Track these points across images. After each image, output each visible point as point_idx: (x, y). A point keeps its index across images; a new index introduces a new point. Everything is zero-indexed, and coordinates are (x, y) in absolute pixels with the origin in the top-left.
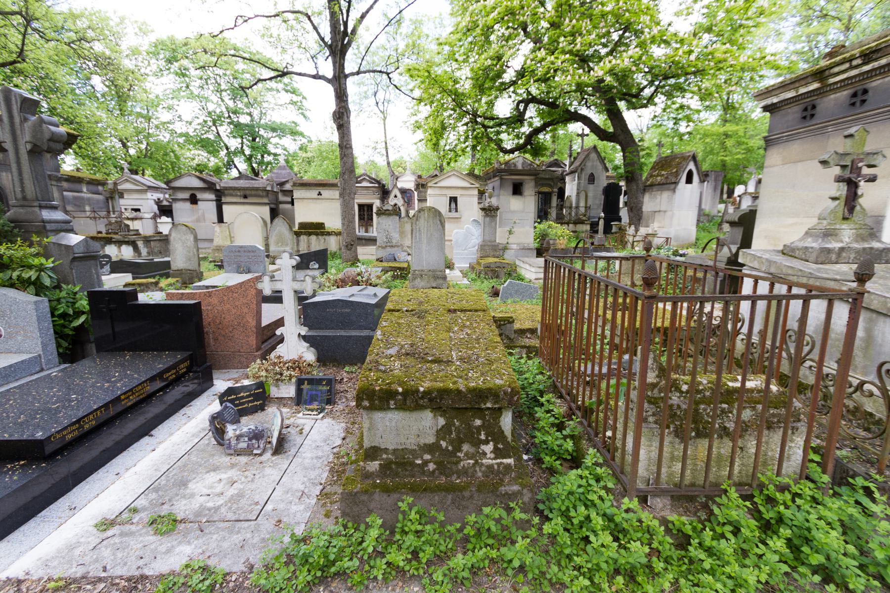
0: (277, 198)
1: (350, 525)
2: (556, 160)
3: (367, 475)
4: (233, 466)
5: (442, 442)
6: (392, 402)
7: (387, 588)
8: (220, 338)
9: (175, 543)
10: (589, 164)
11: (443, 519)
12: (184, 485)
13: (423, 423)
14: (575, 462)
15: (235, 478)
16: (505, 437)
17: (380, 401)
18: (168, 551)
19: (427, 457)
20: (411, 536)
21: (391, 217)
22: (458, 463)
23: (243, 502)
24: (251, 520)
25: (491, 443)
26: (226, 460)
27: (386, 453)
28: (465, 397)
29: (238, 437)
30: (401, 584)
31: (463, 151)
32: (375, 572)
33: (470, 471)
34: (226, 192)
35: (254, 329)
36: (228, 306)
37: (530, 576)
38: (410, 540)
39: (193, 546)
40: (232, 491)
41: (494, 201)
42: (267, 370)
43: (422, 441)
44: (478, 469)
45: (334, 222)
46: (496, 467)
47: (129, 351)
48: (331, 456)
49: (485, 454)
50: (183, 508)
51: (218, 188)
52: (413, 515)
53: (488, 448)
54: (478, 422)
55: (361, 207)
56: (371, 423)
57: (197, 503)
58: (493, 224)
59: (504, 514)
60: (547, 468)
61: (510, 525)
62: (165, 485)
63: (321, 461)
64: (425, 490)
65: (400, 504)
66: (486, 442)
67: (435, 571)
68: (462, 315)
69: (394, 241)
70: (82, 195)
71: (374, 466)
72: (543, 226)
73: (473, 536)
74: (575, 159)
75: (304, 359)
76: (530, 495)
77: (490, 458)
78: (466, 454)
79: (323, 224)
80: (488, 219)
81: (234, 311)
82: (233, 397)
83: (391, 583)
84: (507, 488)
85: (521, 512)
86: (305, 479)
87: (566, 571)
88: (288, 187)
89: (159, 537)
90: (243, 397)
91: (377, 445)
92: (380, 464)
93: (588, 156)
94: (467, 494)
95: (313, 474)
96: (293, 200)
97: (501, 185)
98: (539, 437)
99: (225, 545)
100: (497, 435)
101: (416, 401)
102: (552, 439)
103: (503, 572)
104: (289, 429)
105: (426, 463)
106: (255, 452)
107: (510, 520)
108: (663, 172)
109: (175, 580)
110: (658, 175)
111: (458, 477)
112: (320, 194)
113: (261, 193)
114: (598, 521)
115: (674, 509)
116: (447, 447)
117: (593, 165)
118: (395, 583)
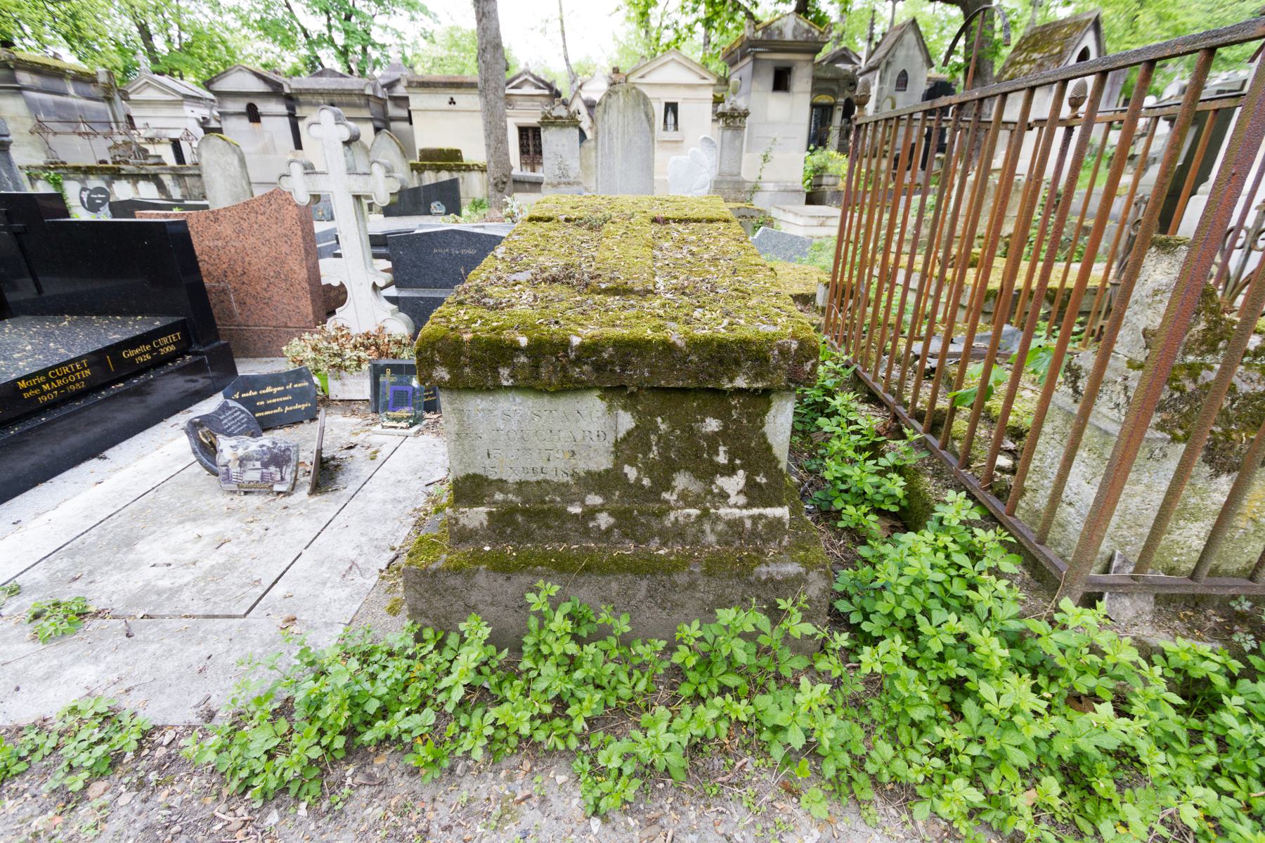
0: (385, 112)
1: (428, 633)
2: (845, 49)
3: (462, 536)
4: (231, 512)
5: (627, 469)
6: (504, 372)
7: (497, 772)
8: (248, 301)
9: (68, 658)
10: (901, 53)
11: (627, 629)
12: (128, 545)
13: (583, 424)
14: (907, 517)
15: (229, 535)
16: (774, 460)
17: (476, 370)
18: (48, 677)
19: (594, 500)
20: (548, 669)
21: (566, 131)
22: (662, 514)
23: (232, 579)
24: (234, 617)
25: (741, 472)
26: (223, 500)
27: (501, 491)
28: (684, 360)
29: (242, 461)
30: (527, 765)
31: (690, 29)
32: (467, 742)
33: (691, 531)
34: (301, 98)
35: (306, 285)
36: (252, 240)
37: (829, 769)
38: (550, 678)
39: (102, 667)
40: (218, 558)
41: (741, 103)
42: (315, 349)
43: (582, 466)
44: (707, 527)
45: (475, 152)
46: (748, 524)
47: (71, 314)
48: (423, 499)
49: (724, 496)
50: (111, 588)
51: (287, 90)
52: (559, 623)
53: (733, 484)
54: (712, 425)
55: (523, 131)
56: (461, 422)
57: (134, 582)
58: (737, 143)
59: (764, 622)
60: (846, 529)
61: (777, 646)
62: (94, 544)
63: (401, 507)
64: (587, 569)
65: (531, 597)
66: (730, 470)
67: (603, 746)
68: (680, 227)
69: (572, 174)
70: (69, 100)
71: (476, 516)
72: (818, 158)
73: (694, 668)
74: (878, 45)
75: (387, 331)
76: (822, 584)
77: (736, 506)
78: (683, 496)
79: (458, 151)
80: (729, 133)
81: (265, 249)
82: (251, 393)
83: (505, 763)
84: (773, 569)
85: (803, 620)
86: (363, 539)
87: (911, 754)
88: (400, 91)
89: (40, 646)
90: (271, 395)
91: (480, 471)
92: (490, 514)
93: (900, 38)
94: (681, 579)
95: (380, 531)
96: (409, 112)
97: (755, 72)
98: (832, 470)
99: (169, 666)
100: (753, 455)
101: (564, 369)
102: (862, 475)
103: (763, 750)
104: (352, 451)
105: (591, 513)
106: (277, 488)
107: (777, 635)
108: (1035, 55)
109: (38, 740)
110: (1025, 62)
111: (664, 544)
112: (452, 102)
113: (356, 100)
114: (993, 650)
115: (1159, 620)
116: (638, 480)
117: (907, 56)
118: (515, 761)
